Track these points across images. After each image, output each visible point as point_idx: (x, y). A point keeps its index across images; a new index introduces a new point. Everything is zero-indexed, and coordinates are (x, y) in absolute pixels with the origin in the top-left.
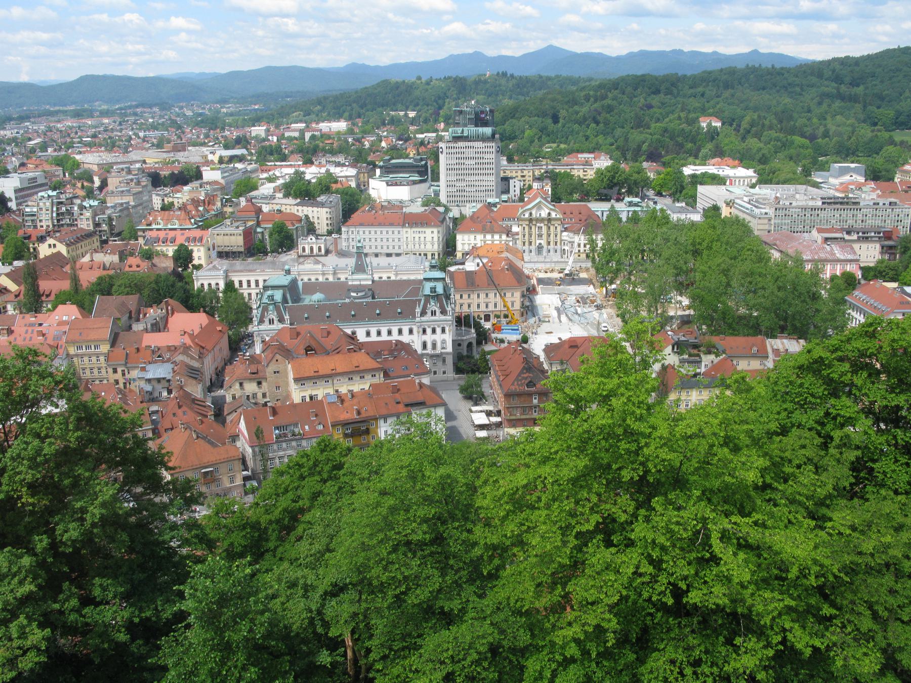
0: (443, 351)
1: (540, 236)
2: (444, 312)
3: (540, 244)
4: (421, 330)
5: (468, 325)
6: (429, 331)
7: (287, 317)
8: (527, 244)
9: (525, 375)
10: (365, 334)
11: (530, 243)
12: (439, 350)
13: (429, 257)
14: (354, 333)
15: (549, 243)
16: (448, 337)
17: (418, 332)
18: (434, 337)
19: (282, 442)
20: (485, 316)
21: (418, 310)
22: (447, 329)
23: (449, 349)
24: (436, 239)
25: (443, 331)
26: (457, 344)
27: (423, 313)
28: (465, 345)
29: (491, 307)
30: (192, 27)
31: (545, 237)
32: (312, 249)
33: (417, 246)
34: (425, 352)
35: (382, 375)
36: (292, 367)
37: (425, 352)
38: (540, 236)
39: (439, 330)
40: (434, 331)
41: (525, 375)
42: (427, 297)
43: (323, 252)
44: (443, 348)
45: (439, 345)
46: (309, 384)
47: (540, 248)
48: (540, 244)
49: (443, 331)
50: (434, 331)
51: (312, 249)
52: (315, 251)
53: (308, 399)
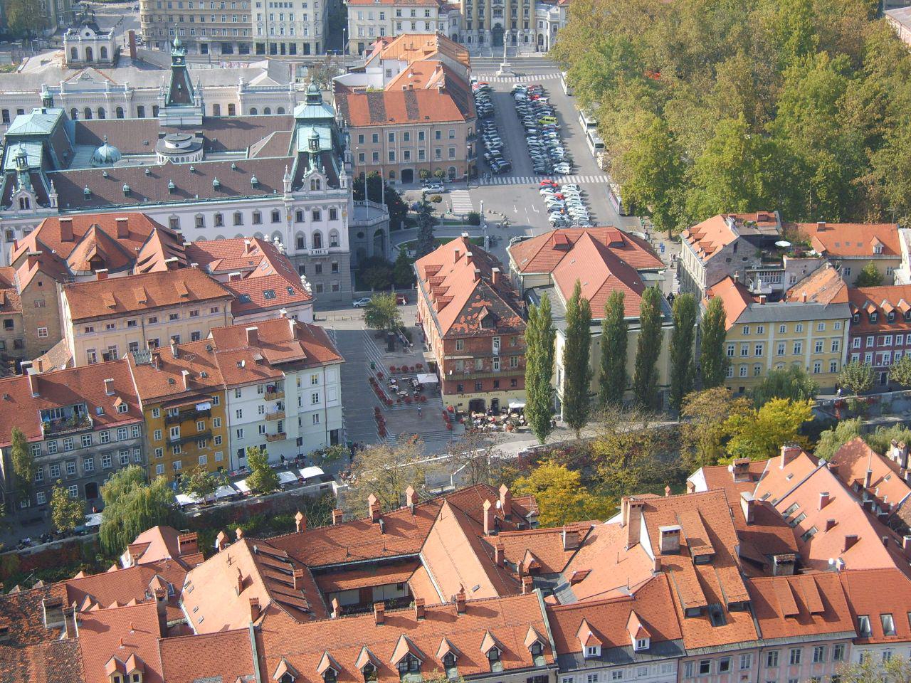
0: (334, 249)
1: (498, 12)
2: (333, 182)
3: (498, 25)
4: (294, 215)
5: (375, 198)
6: (308, 216)
7: (52, 196)
8: (474, 25)
9: (478, 305)
10: (193, 223)
11: (481, 25)
12: (326, 248)
13: (300, 50)
14: (175, 223)
15: (514, 25)
16: (342, 227)
17: (289, 219)
18: (317, 226)
19: (57, 437)
20: (404, 172)
21: (287, 180)
22: (340, 212)
23: (344, 246)
24: (311, 19)
25: (333, 215)
26: (357, 234)
27: (297, 184)
28: (371, 235)
29: (414, 157)
30: (103, 249)
31: (506, 12)
32: (89, 51)
33: (277, 31)
34: (301, 252)
35: (229, 309)
36: (68, 297)
37: (301, 252)
38: (498, 12)
39: (325, 214)
40: (316, 217)
41: (478, 305)
42: (304, 157)
43: (110, 56)
44: (334, 244)
45: (325, 240)
46: (99, 327)
47: (498, 32)
48: (498, 25)
49: (333, 215)
50: (316, 217)
51: (89, 51)
52: (96, 55)
53: (100, 360)
